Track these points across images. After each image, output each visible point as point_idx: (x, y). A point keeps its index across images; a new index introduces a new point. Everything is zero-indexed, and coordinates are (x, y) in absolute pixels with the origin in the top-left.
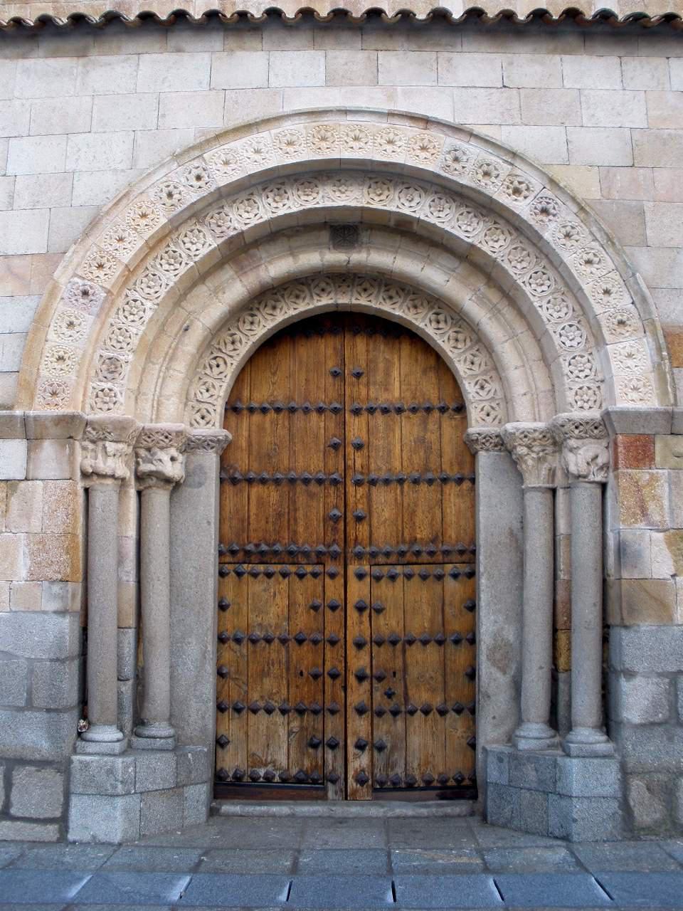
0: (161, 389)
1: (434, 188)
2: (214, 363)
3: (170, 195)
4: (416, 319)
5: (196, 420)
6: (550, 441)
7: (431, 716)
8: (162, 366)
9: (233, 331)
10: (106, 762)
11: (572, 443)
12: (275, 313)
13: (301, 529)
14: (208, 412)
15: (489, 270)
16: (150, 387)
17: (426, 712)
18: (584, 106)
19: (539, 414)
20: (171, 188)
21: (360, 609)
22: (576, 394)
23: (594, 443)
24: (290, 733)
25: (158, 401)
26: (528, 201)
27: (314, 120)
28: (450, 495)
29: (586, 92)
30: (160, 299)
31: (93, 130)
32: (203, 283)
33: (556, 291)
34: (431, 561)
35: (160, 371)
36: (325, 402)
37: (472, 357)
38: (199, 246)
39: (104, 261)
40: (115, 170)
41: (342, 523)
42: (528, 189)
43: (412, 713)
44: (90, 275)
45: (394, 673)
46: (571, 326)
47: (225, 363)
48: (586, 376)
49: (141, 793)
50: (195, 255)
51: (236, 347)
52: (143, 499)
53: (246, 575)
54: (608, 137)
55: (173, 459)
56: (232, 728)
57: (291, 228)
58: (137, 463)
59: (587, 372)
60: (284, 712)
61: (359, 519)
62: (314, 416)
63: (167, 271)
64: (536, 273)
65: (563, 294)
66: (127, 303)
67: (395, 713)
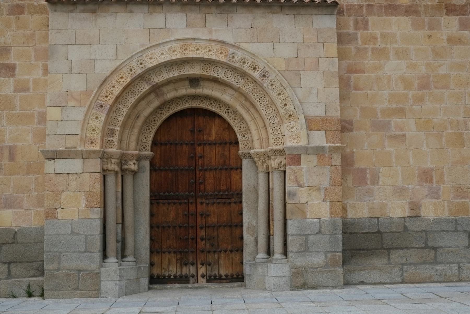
0: (129, 138)
1: (226, 67)
2: (148, 128)
3: (131, 70)
4: (220, 112)
5: (141, 149)
6: (267, 156)
7: (227, 252)
8: (129, 131)
9: (154, 116)
10: (114, 269)
11: (273, 157)
12: (169, 110)
13: (180, 187)
14: (146, 146)
15: (246, 95)
16: (125, 138)
17: (225, 251)
18: (280, 34)
19: (263, 146)
20: (131, 67)
21: (202, 215)
22: (275, 140)
23: (281, 157)
24: (177, 260)
25: (129, 143)
26: (259, 72)
27: (182, 42)
28: (233, 174)
29: (281, 29)
30: (129, 108)
31: (101, 43)
32: (144, 100)
33: (269, 104)
34: (227, 198)
35: (129, 132)
36: (188, 141)
37: (240, 125)
38: (142, 88)
39: (108, 94)
40: (110, 60)
41: (195, 185)
42: (259, 68)
43: (220, 251)
44: (103, 99)
45: (214, 238)
46: (273, 116)
47: (152, 128)
48: (279, 134)
49: (126, 280)
50: (141, 92)
51: (155, 122)
52: (123, 177)
53: (160, 204)
54: (289, 46)
55: (134, 164)
56: (156, 259)
57: (175, 80)
58: (122, 166)
59: (279, 132)
60: (175, 252)
61: (201, 183)
62: (184, 146)
63: (131, 97)
64: (262, 97)
65: (271, 105)
66: (117, 109)
67: (214, 252)
